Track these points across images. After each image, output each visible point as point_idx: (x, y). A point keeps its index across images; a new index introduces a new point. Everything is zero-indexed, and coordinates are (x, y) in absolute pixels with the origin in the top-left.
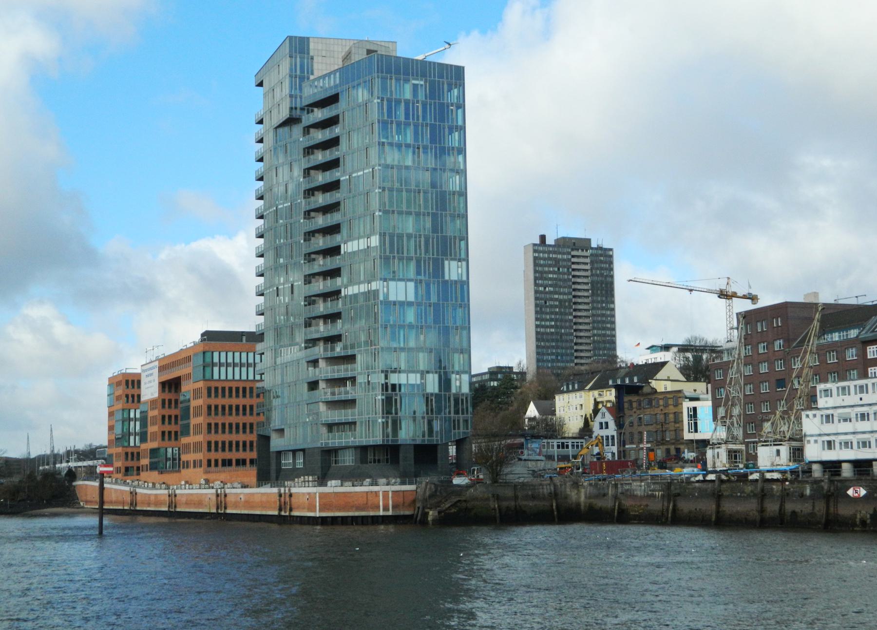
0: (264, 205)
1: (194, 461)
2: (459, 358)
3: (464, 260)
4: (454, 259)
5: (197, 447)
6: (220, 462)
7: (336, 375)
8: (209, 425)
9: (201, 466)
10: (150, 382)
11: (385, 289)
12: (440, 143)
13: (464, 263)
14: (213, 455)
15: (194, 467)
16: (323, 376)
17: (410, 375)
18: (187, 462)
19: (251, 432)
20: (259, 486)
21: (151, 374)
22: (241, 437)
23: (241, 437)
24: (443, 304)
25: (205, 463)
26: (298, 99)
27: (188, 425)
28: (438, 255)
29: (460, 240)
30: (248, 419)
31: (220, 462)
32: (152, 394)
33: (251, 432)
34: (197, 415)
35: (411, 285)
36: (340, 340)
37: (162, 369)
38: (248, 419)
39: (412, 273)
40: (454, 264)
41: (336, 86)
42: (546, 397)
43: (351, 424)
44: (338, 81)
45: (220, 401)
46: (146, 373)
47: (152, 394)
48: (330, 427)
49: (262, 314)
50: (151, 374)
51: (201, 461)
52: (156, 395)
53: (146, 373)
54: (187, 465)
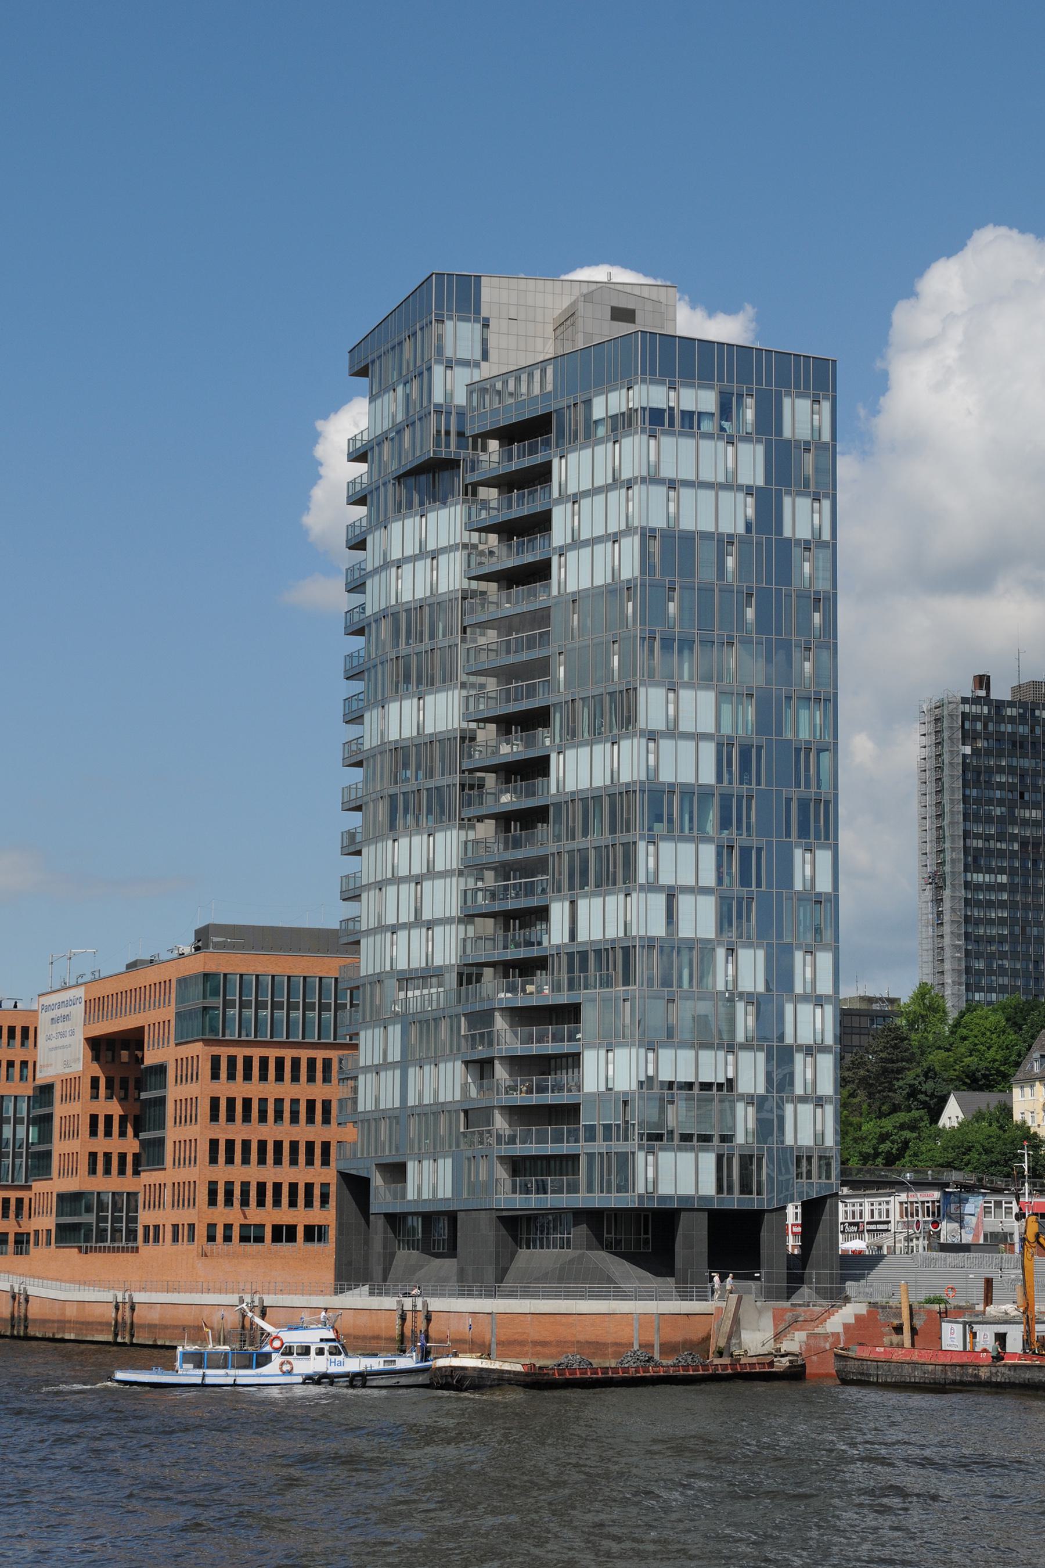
0: (370, 472)
1: (175, 1227)
2: (812, 718)
3: (826, 496)
4: (805, 494)
5: (183, 1196)
6: (236, 1233)
7: (535, 1049)
8: (214, 1144)
9: (192, 1238)
10: (62, 1035)
11: (651, 757)
12: (779, 632)
13: (826, 504)
14: (222, 1215)
15: (175, 1239)
16: (505, 1100)
17: (701, 1053)
18: (157, 1227)
19: (326, 1162)
20: (339, 1290)
21: (65, 1018)
22: (302, 1174)
23: (302, 1174)
24: (779, 895)
25: (201, 1232)
26: (453, 419)
27: (161, 1142)
28: (769, 783)
29: (819, 751)
30: (316, 1133)
31: (236, 1233)
32: (66, 1064)
33: (326, 1162)
34: (186, 1119)
35: (708, 852)
36: (545, 820)
37: (95, 1006)
38: (316, 1133)
39: (711, 826)
40: (804, 503)
41: (545, 396)
42: (993, 1078)
43: (568, 1163)
44: (549, 387)
45: (238, 1131)
46: (53, 1014)
47: (66, 1064)
48: (518, 1166)
49: (359, 808)
50: (65, 1018)
51: (192, 1226)
52: (78, 1067)
53: (53, 1014)
54: (154, 1234)
